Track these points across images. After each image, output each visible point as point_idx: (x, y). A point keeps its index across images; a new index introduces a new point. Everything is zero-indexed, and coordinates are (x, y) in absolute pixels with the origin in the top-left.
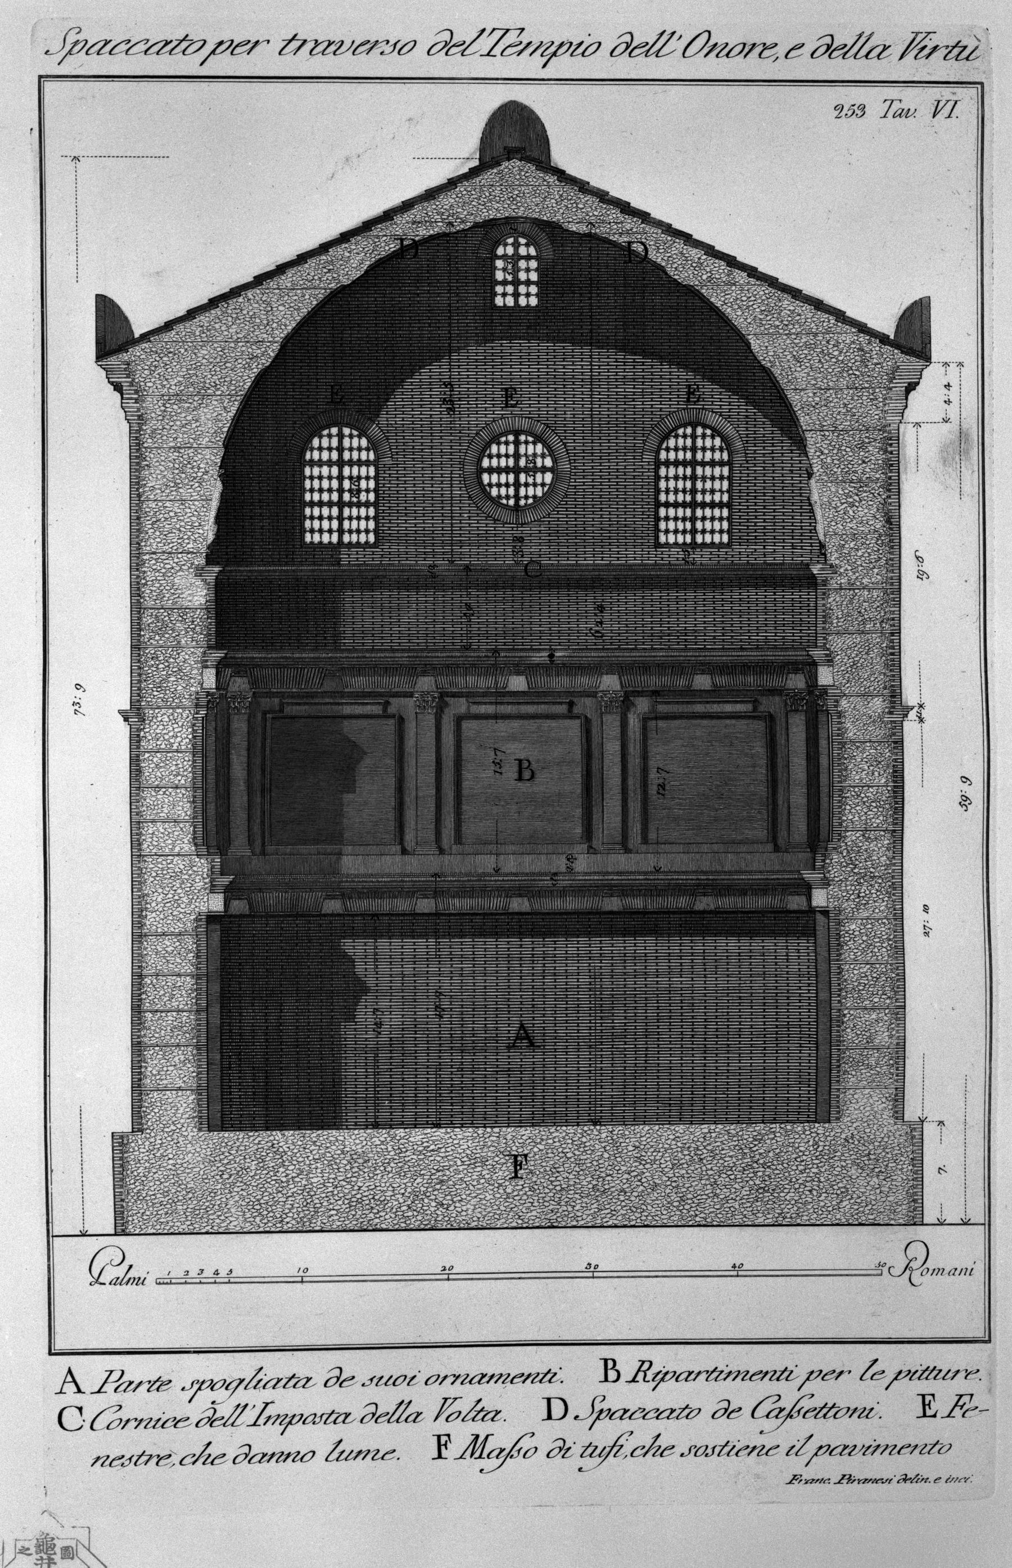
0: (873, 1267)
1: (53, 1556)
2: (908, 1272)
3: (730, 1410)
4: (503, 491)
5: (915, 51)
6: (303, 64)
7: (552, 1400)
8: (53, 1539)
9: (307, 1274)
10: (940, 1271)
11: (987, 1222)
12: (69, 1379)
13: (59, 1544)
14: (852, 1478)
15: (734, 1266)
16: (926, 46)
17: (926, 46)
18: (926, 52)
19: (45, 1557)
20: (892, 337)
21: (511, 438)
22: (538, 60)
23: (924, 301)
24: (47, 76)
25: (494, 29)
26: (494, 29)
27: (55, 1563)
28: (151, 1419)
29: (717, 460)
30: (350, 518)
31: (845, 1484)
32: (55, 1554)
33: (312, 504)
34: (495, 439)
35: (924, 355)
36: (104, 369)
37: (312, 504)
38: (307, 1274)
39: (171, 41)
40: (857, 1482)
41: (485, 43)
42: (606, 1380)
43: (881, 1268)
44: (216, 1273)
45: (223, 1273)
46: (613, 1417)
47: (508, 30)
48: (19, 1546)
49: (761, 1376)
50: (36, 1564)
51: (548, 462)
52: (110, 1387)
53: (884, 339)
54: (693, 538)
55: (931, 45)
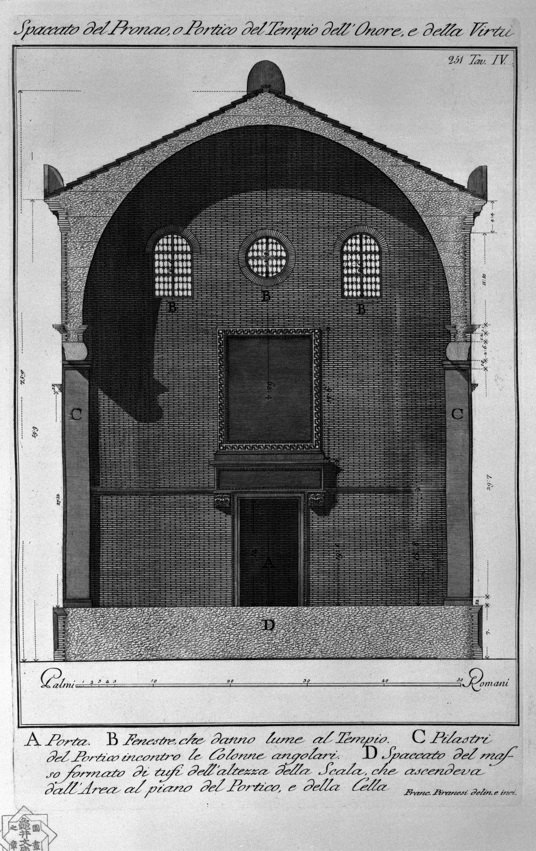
0: (302, 682)
1: (28, 830)
2: (471, 684)
3: (285, 770)
4: (260, 270)
5: (479, 31)
6: (126, 38)
7: (369, 747)
8: (28, 821)
9: (155, 683)
10: (488, 684)
11: (19, 663)
12: (32, 738)
13: (32, 824)
14: (442, 791)
15: (383, 681)
16: (483, 30)
17: (483, 30)
18: (483, 32)
19: (24, 830)
20: (466, 187)
21: (264, 240)
22: (290, 36)
23: (483, 168)
24: (517, 51)
25: (272, 22)
26: (272, 22)
27: (30, 834)
28: (247, 754)
29: (161, 251)
30: (367, 283)
31: (438, 795)
32: (30, 829)
33: (159, 275)
34: (256, 241)
35: (484, 196)
36: (48, 204)
37: (159, 275)
38: (155, 683)
39: (66, 28)
40: (444, 794)
41: (267, 29)
42: (110, 744)
43: (460, 682)
44: (108, 682)
45: (111, 682)
46: (401, 757)
47: (277, 23)
48: (10, 826)
49: (138, 742)
50: (20, 835)
51: (284, 254)
52: (54, 743)
53: (461, 188)
54: (173, 293)
55: (486, 29)
